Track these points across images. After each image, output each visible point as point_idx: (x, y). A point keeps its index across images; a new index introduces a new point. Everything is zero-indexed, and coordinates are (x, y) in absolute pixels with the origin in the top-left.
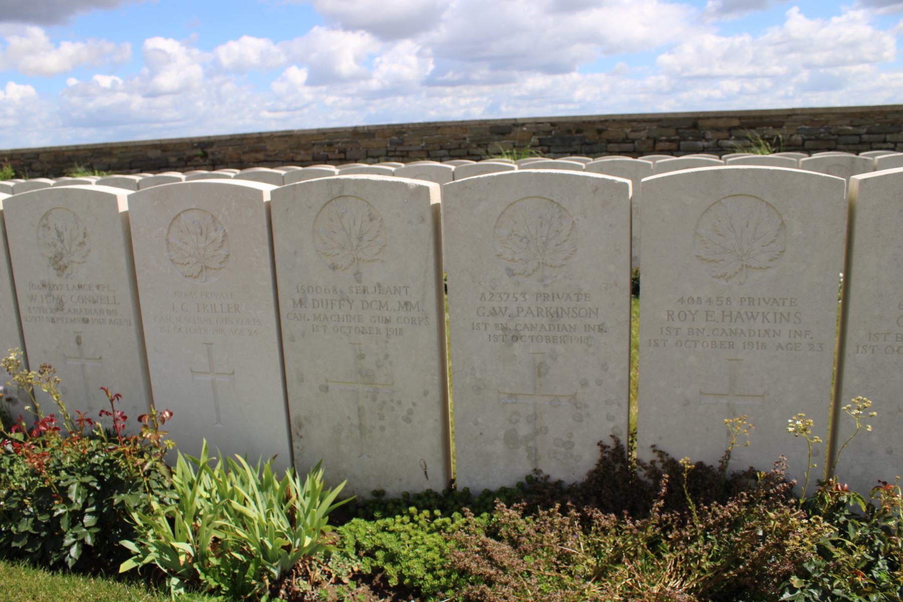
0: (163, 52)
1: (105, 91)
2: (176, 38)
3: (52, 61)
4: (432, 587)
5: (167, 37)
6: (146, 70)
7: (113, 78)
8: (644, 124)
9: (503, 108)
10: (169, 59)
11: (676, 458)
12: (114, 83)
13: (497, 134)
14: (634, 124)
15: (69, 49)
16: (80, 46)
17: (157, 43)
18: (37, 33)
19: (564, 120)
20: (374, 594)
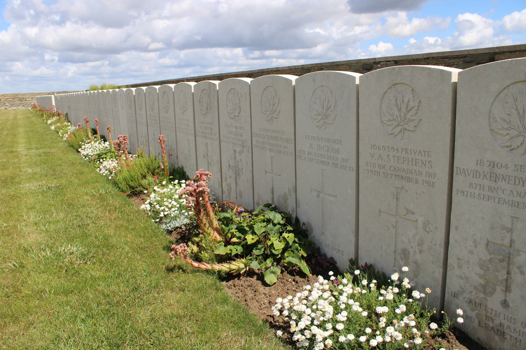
0: (469, 21)
1: (431, 45)
2: (479, 14)
3: (407, 29)
4: (222, 311)
5: (472, 12)
6: (457, 33)
7: (435, 38)
8: (453, 61)
9: (350, 50)
10: (471, 25)
11: (387, 272)
12: (436, 41)
13: (366, 70)
14: (447, 60)
15: (416, 22)
16: (422, 20)
17: (468, 16)
18: (402, 15)
19: (402, 59)
20: (366, 264)
